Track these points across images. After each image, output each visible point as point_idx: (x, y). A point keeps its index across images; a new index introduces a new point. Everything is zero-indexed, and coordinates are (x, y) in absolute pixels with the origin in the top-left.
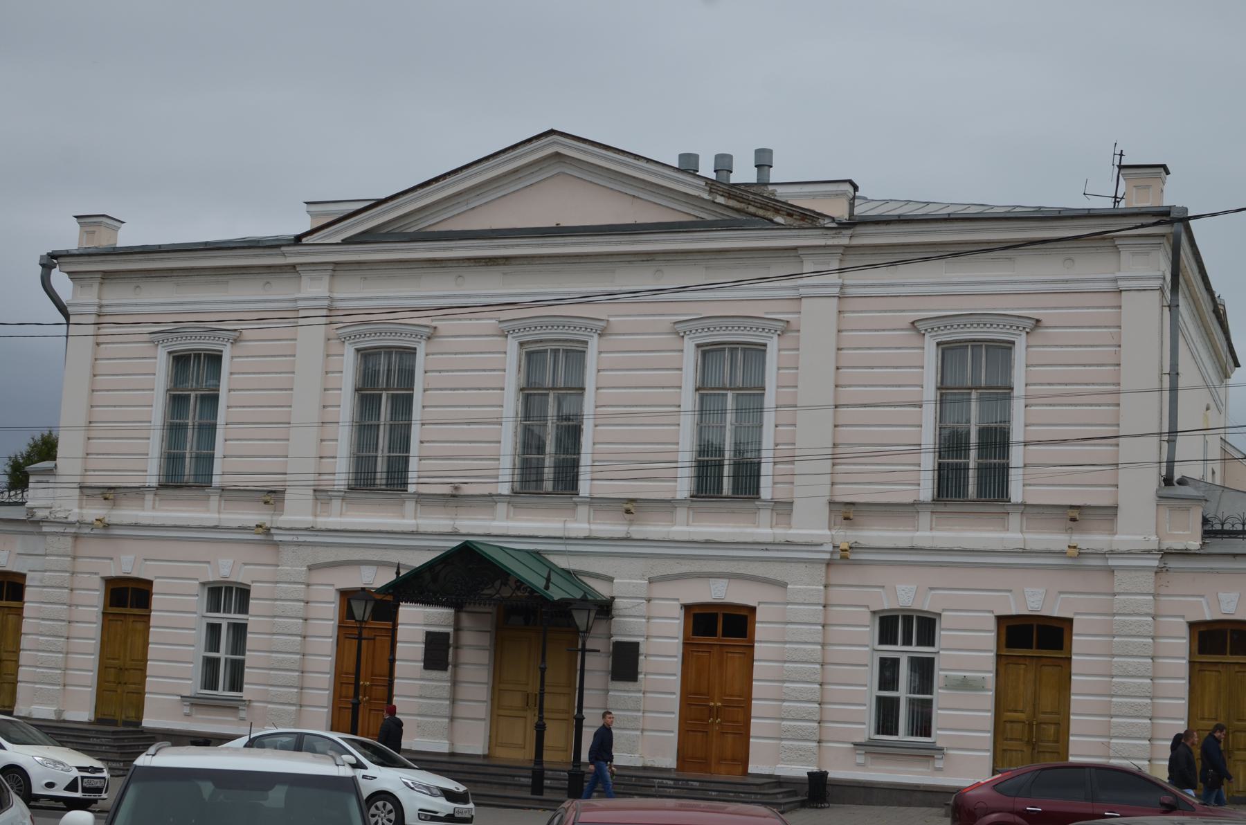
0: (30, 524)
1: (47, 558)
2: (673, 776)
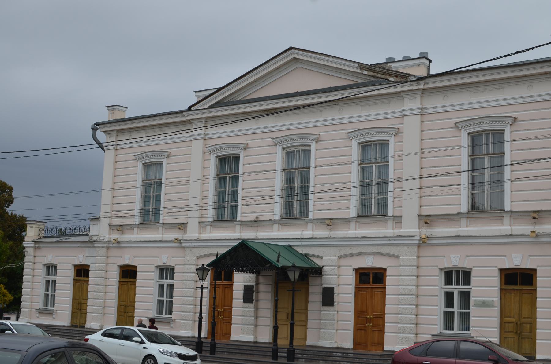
0: (89, 243)
1: (97, 258)
2: (352, 352)
